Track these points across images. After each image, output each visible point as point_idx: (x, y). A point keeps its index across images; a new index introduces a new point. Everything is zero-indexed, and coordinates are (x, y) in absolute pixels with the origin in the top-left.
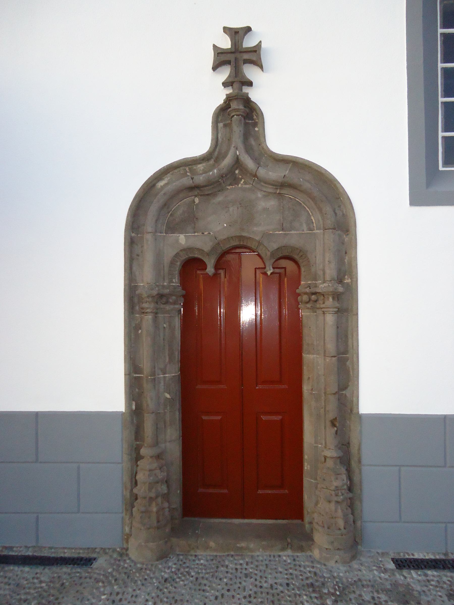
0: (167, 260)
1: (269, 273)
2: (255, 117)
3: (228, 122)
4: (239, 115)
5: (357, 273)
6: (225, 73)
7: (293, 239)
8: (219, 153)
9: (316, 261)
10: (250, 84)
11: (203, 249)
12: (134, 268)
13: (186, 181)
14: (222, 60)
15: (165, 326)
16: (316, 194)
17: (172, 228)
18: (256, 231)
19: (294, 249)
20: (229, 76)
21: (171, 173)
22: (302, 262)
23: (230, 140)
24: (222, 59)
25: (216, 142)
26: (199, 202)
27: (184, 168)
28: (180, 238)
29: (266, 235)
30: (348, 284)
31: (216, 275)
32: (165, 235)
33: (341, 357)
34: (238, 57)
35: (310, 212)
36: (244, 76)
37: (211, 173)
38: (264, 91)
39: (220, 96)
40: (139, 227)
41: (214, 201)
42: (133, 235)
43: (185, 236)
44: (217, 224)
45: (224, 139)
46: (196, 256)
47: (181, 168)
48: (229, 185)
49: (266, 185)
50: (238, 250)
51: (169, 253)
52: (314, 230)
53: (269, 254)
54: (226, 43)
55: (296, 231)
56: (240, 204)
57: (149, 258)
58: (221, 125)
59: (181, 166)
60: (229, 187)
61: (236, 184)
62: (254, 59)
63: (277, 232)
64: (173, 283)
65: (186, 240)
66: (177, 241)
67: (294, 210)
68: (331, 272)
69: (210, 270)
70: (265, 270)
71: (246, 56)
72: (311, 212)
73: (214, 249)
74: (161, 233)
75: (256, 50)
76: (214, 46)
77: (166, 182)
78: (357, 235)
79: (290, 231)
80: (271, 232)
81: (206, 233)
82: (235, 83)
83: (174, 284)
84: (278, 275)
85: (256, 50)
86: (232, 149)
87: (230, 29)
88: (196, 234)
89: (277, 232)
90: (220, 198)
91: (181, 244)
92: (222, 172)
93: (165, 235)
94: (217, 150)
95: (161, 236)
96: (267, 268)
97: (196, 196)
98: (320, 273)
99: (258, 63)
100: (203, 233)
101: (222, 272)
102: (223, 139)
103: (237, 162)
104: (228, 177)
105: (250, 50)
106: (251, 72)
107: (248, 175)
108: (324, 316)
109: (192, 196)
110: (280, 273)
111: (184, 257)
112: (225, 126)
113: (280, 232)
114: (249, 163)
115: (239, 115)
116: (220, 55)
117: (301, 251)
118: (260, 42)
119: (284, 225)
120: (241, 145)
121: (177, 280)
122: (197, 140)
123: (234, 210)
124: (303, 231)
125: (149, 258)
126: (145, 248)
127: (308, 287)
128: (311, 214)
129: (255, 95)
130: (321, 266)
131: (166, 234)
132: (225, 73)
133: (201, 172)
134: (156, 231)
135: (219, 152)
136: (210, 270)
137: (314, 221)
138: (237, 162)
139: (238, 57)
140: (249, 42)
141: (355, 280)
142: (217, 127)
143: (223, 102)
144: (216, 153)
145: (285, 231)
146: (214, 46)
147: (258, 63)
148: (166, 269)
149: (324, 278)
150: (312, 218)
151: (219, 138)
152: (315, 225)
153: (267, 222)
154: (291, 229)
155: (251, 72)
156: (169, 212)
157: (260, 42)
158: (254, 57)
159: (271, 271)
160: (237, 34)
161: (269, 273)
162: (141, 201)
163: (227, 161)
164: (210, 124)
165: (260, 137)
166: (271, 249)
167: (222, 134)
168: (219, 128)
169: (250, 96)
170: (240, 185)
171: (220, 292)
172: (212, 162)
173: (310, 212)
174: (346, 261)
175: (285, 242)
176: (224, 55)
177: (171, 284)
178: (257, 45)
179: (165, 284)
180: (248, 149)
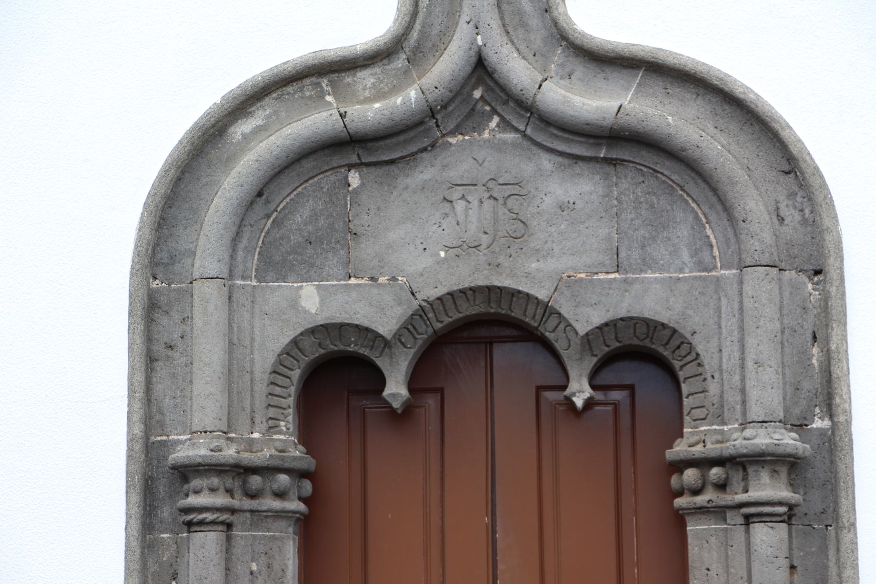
1: (579, 402)
11: (373, 327)
12: (159, 388)
15: (254, 567)
17: (277, 264)
19: (652, 326)
21: (274, 95)
22: (682, 367)
26: (363, 185)
29: (565, 283)
30: (822, 432)
33: (645, 278)
35: (699, 212)
37: (399, 101)
41: (409, 181)
42: (155, 284)
43: (318, 288)
44: (411, 253)
46: (352, 348)
47: (307, 81)
49: (566, 136)
50: (484, 332)
51: (271, 338)
52: (715, 268)
55: (661, 270)
57: (208, 352)
59: (306, 76)
60: (453, 140)
61: (474, 129)
63: (602, 276)
65: (322, 300)
66: (294, 304)
68: (766, 393)
69: (396, 389)
72: (704, 214)
73: (408, 327)
74: (244, 278)
77: (260, 122)
78: (846, 285)
79: (641, 271)
80: (583, 275)
81: (382, 280)
84: (610, 408)
86: (463, 31)
88: (353, 281)
89: (602, 276)
91: (306, 312)
92: (431, 98)
94: (417, 26)
96: (573, 386)
97: (350, 167)
98: (733, 398)
100: (372, 279)
103: (481, 68)
104: (450, 109)
108: (747, 531)
114: (517, 70)
117: (675, 331)
119: (623, 254)
125: (208, 352)
127: (726, 550)
128: (704, 220)
131: (259, 281)
133: (367, 94)
134: (231, 276)
135: (422, 32)
136: (396, 389)
137: (714, 241)
138: (481, 68)
141: (842, 418)
144: (414, 35)
145: (626, 272)
148: (261, 388)
149: (744, 413)
150: (709, 232)
152: (716, 252)
153: (577, 256)
154: (646, 264)
156: (268, 216)
161: (579, 402)
162: (179, 179)
163: (447, 66)
166: (582, 329)
170: (486, 135)
171: (189, 549)
172: (400, 62)
173: (699, 212)
175: (625, 305)
177: (275, 437)
179: (256, 435)
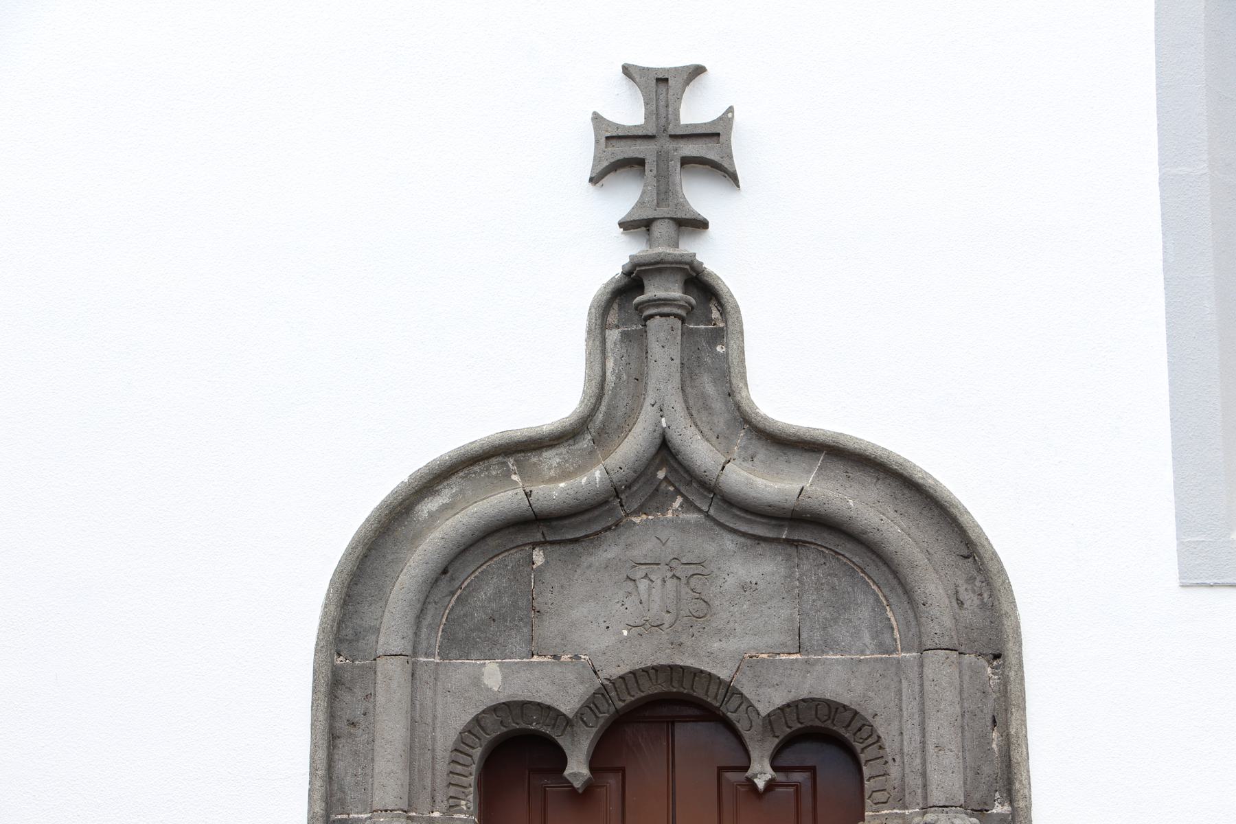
0: (445, 736)
1: (760, 783)
2: (715, 314)
3: (634, 327)
4: (666, 304)
5: (1023, 691)
6: (625, 197)
7: (834, 677)
8: (609, 416)
9: (902, 744)
10: (700, 225)
12: (340, 766)
13: (503, 498)
14: (620, 157)
16: (870, 532)
17: (459, 642)
18: (715, 654)
19: (834, 708)
20: (641, 204)
23: (640, 379)
24: (620, 155)
25: (599, 392)
26: (547, 562)
27: (500, 459)
28: (486, 670)
29: (747, 663)
31: (590, 788)
32: (437, 660)
34: (664, 151)
35: (892, 619)
36: (684, 204)
37: (584, 480)
38: (734, 244)
39: (615, 255)
40: (357, 636)
41: (592, 559)
42: (339, 661)
43: (501, 665)
44: (593, 632)
45: (624, 377)
46: (533, 727)
48: (637, 512)
50: (665, 711)
51: (453, 715)
52: (896, 650)
53: (758, 722)
54: (629, 112)
55: (842, 652)
56: (671, 569)
58: (613, 335)
59: (493, 456)
60: (636, 520)
61: (657, 509)
62: (712, 156)
63: (783, 657)
64: (461, 812)
65: (505, 678)
66: (477, 681)
67: (833, 588)
69: (577, 768)
70: (749, 773)
71: (691, 149)
73: (591, 705)
74: (427, 655)
75: (715, 134)
76: (597, 118)
77: (446, 501)
79: (823, 652)
81: (565, 658)
82: (658, 223)
83: (462, 816)
85: (715, 134)
87: (644, 71)
88: (536, 659)
89: (783, 657)
90: (609, 551)
91: (488, 689)
93: (437, 660)
94: (603, 408)
95: (426, 664)
96: (755, 767)
97: (535, 545)
98: (914, 781)
99: (725, 173)
101: (613, 781)
102: (619, 377)
105: (699, 131)
106: (700, 196)
107: (694, 485)
109: (525, 545)
110: (797, 787)
111: (495, 730)
112: (626, 336)
113: (794, 657)
114: (701, 451)
115: (666, 304)
116: (614, 142)
117: (856, 713)
118: (731, 109)
119: (804, 635)
120: (675, 402)
121: (471, 805)
122: (546, 383)
123: (656, 595)
124: (862, 653)
125: (390, 730)
126: (381, 699)
129: (713, 255)
130: (918, 761)
132: (625, 197)
133: (552, 473)
134: (415, 653)
136: (577, 768)
137: (894, 623)
138: (665, 450)
139: (664, 151)
140: (695, 110)
142: (604, 341)
143: (620, 271)
144: (600, 416)
146: (597, 118)
147: (723, 171)
149: (925, 798)
150: (890, 614)
151: (609, 373)
152: (897, 635)
153: (757, 634)
154: (828, 645)
155: (700, 196)
156: (453, 593)
157: (731, 109)
158: (709, 154)
159: (768, 776)
160: (662, 85)
161: (760, 783)
163: (632, 446)
164: (582, 334)
165: (728, 376)
167: (616, 360)
168: (609, 344)
169: (698, 258)
170: (670, 515)
172: (585, 442)
174: (994, 746)
176: (622, 143)
178: (720, 118)
179: (436, 814)
180: (695, 408)
